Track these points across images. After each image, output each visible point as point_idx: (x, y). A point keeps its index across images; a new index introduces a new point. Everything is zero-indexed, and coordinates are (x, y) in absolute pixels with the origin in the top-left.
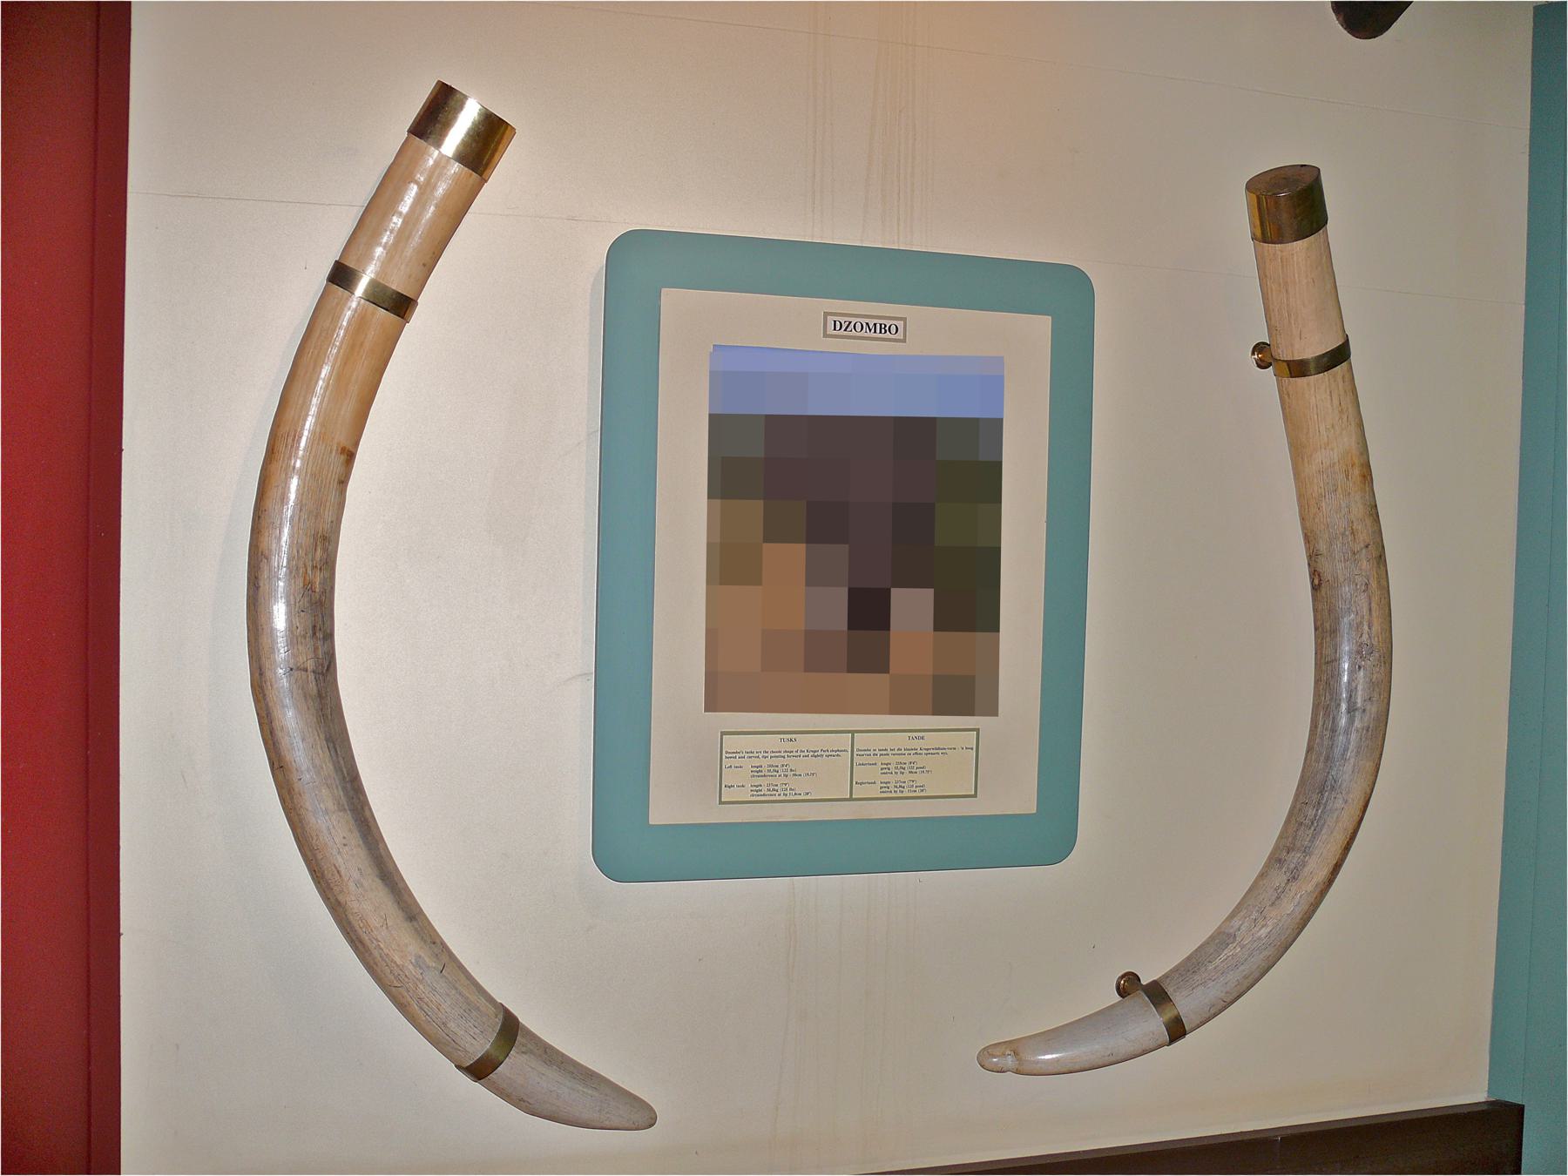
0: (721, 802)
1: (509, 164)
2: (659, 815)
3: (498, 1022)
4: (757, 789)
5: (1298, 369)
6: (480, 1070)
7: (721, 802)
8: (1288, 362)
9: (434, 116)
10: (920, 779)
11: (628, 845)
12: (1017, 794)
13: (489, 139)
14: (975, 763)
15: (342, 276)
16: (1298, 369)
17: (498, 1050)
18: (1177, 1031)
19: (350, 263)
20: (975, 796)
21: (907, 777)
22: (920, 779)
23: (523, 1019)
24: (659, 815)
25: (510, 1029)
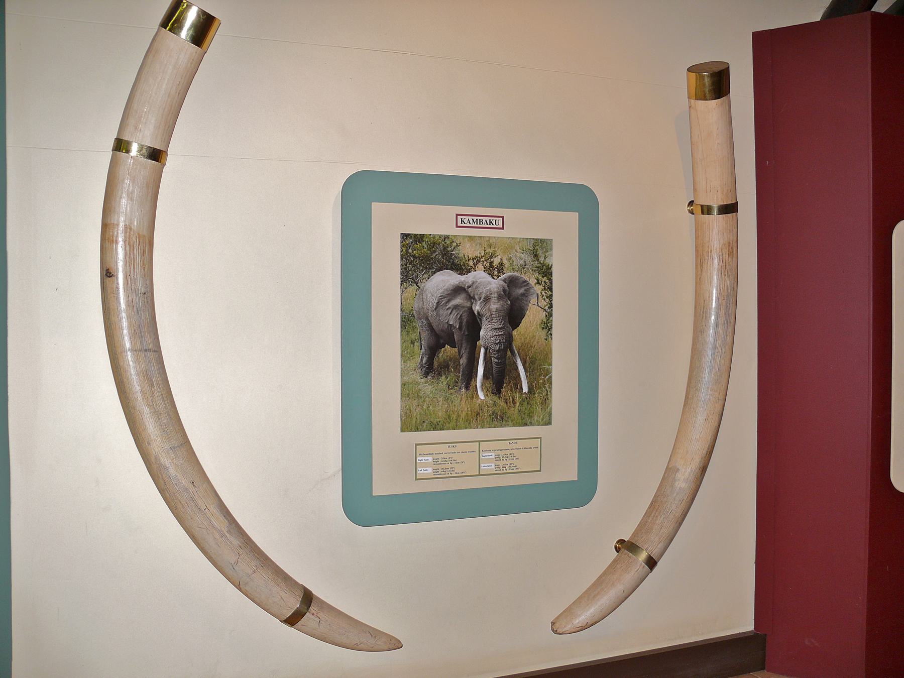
0: (416, 479)
1: (217, 39)
2: (377, 491)
3: (300, 594)
4: (435, 471)
5: (707, 210)
6: (292, 621)
7: (416, 479)
8: (702, 206)
9: (171, 21)
10: (515, 462)
11: (363, 505)
12: (567, 471)
13: (204, 28)
14: (539, 450)
15: (121, 146)
16: (707, 210)
17: (303, 609)
18: (651, 563)
19: (126, 138)
20: (416, 445)
21: (508, 462)
22: (515, 462)
23: (315, 592)
24: (377, 491)
25: (308, 598)
